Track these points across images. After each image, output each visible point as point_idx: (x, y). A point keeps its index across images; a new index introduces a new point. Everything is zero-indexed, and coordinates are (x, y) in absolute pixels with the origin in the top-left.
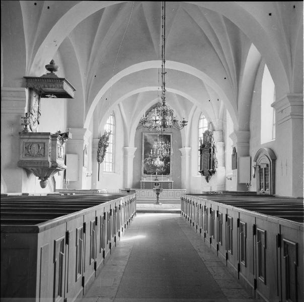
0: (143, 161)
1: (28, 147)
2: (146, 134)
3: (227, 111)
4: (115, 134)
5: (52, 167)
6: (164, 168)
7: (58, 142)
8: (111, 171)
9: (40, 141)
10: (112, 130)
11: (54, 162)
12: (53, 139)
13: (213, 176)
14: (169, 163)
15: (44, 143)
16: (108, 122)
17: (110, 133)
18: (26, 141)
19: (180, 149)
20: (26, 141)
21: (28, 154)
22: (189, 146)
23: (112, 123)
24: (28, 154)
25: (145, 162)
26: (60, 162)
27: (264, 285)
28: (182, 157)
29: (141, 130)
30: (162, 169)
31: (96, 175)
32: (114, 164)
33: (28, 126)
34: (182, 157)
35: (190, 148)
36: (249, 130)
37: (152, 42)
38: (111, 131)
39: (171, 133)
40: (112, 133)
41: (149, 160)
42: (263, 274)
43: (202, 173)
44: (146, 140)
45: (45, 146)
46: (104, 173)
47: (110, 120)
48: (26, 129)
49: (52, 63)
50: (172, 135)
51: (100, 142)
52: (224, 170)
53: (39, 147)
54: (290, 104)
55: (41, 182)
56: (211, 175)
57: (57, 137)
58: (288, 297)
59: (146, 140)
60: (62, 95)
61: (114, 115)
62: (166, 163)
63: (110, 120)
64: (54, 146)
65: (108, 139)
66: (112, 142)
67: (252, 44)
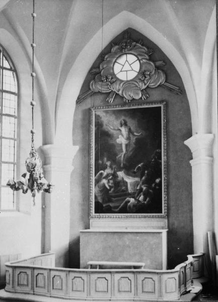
0: (93, 178)
2: (100, 113)
3: (142, 164)
6: (146, 195)
14: (158, 181)
25: (97, 181)
28: (191, 162)
29: (88, 103)
30: (141, 198)
34: (191, 162)
35: (211, 136)
36: (212, 156)
37: (95, 196)
39: (161, 102)
41: (108, 175)
44: (99, 125)
50: (167, 106)
59: (99, 125)
60: (20, 123)
62: (149, 181)
67: (118, 173)
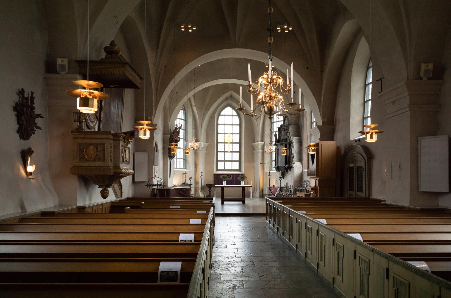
1: (82, 149)
4: (186, 130)
5: (115, 173)
7: (121, 143)
8: (182, 167)
9: (98, 141)
10: (183, 124)
11: (117, 167)
12: (115, 138)
13: (289, 172)
15: (104, 144)
16: (179, 116)
17: (180, 128)
18: (80, 141)
19: (253, 144)
20: (80, 141)
21: (82, 158)
22: (262, 141)
23: (183, 118)
24: (82, 158)
26: (125, 167)
27: (342, 283)
31: (167, 172)
32: (185, 160)
33: (84, 124)
35: (263, 143)
38: (181, 125)
40: (182, 127)
42: (323, 260)
43: (278, 169)
45: (104, 147)
46: (175, 169)
47: (181, 115)
48: (80, 127)
49: (112, 43)
51: (170, 138)
52: (301, 166)
53: (97, 149)
54: (407, 94)
55: (101, 192)
56: (287, 171)
57: (120, 136)
58: (362, 293)
61: (185, 110)
63: (181, 115)
64: (116, 147)
65: (178, 133)
66: (182, 137)
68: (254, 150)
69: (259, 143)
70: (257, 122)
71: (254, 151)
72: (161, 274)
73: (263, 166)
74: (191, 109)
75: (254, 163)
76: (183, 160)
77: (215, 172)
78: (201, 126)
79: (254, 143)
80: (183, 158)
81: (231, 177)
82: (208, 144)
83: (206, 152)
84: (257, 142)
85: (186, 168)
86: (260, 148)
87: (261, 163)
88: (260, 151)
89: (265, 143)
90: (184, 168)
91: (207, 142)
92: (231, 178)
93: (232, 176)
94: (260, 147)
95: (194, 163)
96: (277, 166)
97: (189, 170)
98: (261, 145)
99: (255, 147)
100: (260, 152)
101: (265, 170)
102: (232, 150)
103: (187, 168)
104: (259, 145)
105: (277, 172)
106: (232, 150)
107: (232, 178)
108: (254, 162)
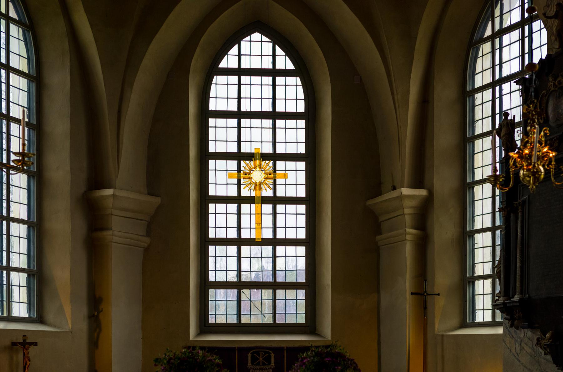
19: (370, 202)
22: (418, 183)
35: (423, 192)
68: (380, 233)
69: (406, 191)
70: (393, 94)
71: (378, 238)
72: (321, 347)
73: (425, 308)
74: (61, 25)
75: (378, 292)
76: (29, 276)
77: (191, 338)
78: (119, 112)
79: (379, 194)
80: (29, 266)
81: (268, 360)
82: (156, 201)
83: (147, 240)
84: (394, 188)
85: (40, 319)
86: (408, 220)
87: (414, 292)
88: (411, 233)
89: (431, 193)
90: (34, 315)
91: (149, 194)
92: (270, 363)
93: (273, 355)
94: (408, 210)
95: (83, 292)
96: (517, 298)
97: (54, 326)
98: (413, 203)
99: (381, 219)
100: (408, 237)
101: (434, 324)
102: (251, 120)
103: (50, 316)
104: (408, 203)
105: (512, 330)
106: (251, 120)
107: (273, 364)
108: (377, 288)
